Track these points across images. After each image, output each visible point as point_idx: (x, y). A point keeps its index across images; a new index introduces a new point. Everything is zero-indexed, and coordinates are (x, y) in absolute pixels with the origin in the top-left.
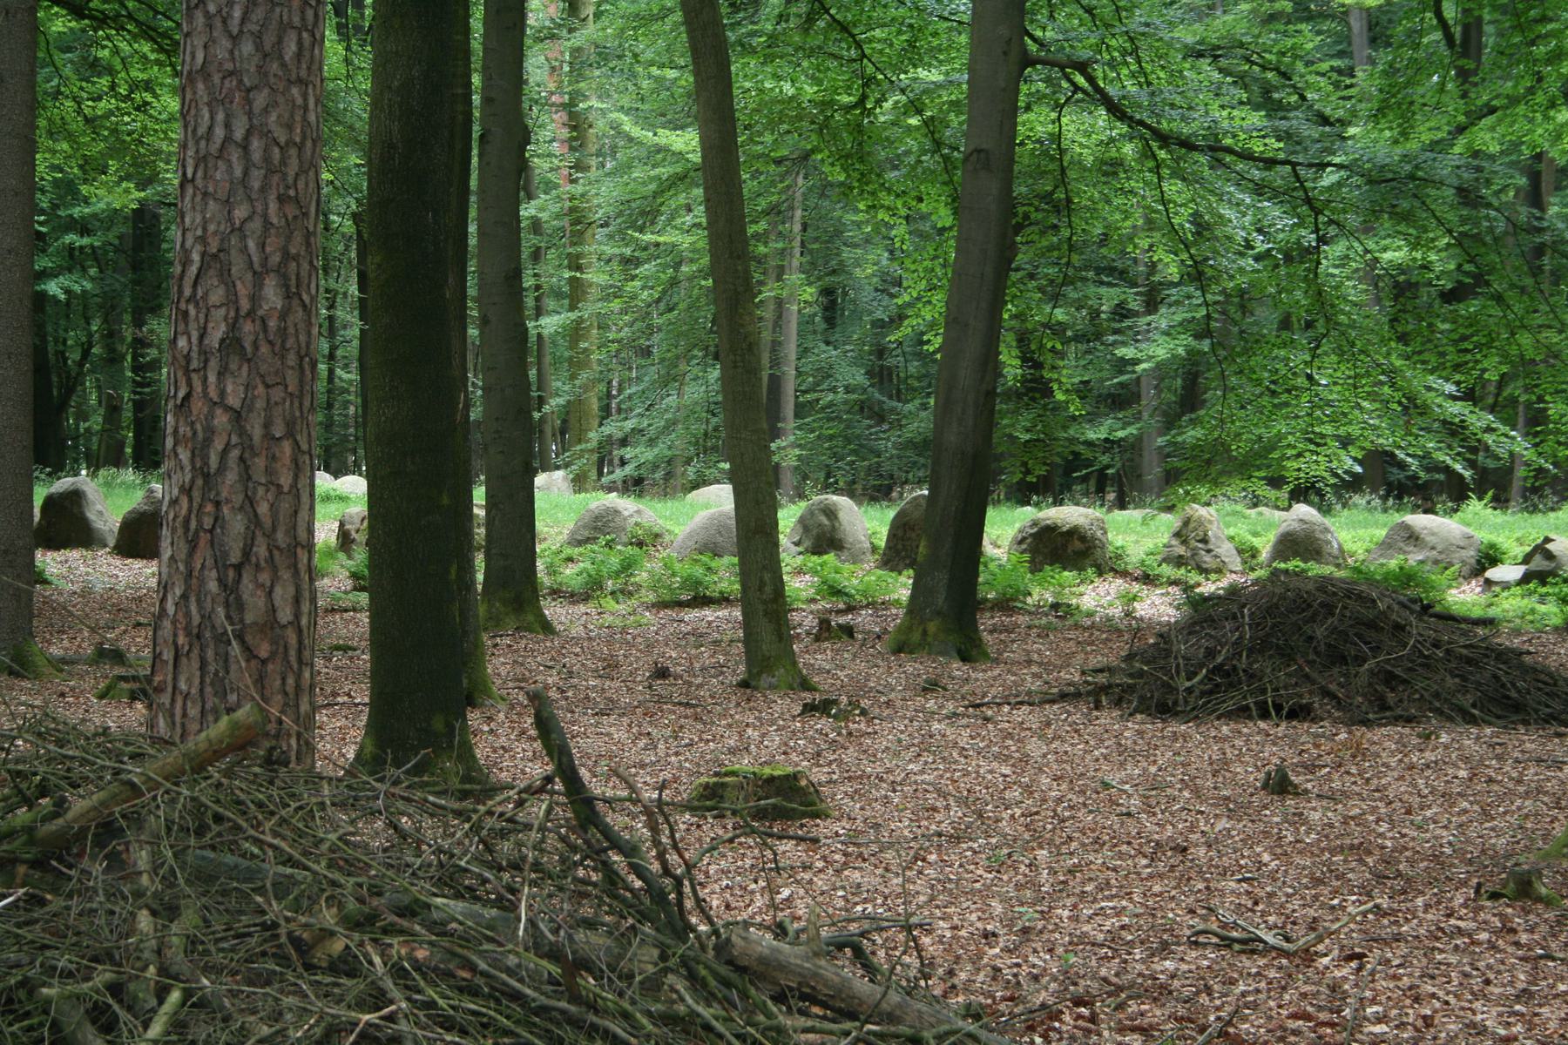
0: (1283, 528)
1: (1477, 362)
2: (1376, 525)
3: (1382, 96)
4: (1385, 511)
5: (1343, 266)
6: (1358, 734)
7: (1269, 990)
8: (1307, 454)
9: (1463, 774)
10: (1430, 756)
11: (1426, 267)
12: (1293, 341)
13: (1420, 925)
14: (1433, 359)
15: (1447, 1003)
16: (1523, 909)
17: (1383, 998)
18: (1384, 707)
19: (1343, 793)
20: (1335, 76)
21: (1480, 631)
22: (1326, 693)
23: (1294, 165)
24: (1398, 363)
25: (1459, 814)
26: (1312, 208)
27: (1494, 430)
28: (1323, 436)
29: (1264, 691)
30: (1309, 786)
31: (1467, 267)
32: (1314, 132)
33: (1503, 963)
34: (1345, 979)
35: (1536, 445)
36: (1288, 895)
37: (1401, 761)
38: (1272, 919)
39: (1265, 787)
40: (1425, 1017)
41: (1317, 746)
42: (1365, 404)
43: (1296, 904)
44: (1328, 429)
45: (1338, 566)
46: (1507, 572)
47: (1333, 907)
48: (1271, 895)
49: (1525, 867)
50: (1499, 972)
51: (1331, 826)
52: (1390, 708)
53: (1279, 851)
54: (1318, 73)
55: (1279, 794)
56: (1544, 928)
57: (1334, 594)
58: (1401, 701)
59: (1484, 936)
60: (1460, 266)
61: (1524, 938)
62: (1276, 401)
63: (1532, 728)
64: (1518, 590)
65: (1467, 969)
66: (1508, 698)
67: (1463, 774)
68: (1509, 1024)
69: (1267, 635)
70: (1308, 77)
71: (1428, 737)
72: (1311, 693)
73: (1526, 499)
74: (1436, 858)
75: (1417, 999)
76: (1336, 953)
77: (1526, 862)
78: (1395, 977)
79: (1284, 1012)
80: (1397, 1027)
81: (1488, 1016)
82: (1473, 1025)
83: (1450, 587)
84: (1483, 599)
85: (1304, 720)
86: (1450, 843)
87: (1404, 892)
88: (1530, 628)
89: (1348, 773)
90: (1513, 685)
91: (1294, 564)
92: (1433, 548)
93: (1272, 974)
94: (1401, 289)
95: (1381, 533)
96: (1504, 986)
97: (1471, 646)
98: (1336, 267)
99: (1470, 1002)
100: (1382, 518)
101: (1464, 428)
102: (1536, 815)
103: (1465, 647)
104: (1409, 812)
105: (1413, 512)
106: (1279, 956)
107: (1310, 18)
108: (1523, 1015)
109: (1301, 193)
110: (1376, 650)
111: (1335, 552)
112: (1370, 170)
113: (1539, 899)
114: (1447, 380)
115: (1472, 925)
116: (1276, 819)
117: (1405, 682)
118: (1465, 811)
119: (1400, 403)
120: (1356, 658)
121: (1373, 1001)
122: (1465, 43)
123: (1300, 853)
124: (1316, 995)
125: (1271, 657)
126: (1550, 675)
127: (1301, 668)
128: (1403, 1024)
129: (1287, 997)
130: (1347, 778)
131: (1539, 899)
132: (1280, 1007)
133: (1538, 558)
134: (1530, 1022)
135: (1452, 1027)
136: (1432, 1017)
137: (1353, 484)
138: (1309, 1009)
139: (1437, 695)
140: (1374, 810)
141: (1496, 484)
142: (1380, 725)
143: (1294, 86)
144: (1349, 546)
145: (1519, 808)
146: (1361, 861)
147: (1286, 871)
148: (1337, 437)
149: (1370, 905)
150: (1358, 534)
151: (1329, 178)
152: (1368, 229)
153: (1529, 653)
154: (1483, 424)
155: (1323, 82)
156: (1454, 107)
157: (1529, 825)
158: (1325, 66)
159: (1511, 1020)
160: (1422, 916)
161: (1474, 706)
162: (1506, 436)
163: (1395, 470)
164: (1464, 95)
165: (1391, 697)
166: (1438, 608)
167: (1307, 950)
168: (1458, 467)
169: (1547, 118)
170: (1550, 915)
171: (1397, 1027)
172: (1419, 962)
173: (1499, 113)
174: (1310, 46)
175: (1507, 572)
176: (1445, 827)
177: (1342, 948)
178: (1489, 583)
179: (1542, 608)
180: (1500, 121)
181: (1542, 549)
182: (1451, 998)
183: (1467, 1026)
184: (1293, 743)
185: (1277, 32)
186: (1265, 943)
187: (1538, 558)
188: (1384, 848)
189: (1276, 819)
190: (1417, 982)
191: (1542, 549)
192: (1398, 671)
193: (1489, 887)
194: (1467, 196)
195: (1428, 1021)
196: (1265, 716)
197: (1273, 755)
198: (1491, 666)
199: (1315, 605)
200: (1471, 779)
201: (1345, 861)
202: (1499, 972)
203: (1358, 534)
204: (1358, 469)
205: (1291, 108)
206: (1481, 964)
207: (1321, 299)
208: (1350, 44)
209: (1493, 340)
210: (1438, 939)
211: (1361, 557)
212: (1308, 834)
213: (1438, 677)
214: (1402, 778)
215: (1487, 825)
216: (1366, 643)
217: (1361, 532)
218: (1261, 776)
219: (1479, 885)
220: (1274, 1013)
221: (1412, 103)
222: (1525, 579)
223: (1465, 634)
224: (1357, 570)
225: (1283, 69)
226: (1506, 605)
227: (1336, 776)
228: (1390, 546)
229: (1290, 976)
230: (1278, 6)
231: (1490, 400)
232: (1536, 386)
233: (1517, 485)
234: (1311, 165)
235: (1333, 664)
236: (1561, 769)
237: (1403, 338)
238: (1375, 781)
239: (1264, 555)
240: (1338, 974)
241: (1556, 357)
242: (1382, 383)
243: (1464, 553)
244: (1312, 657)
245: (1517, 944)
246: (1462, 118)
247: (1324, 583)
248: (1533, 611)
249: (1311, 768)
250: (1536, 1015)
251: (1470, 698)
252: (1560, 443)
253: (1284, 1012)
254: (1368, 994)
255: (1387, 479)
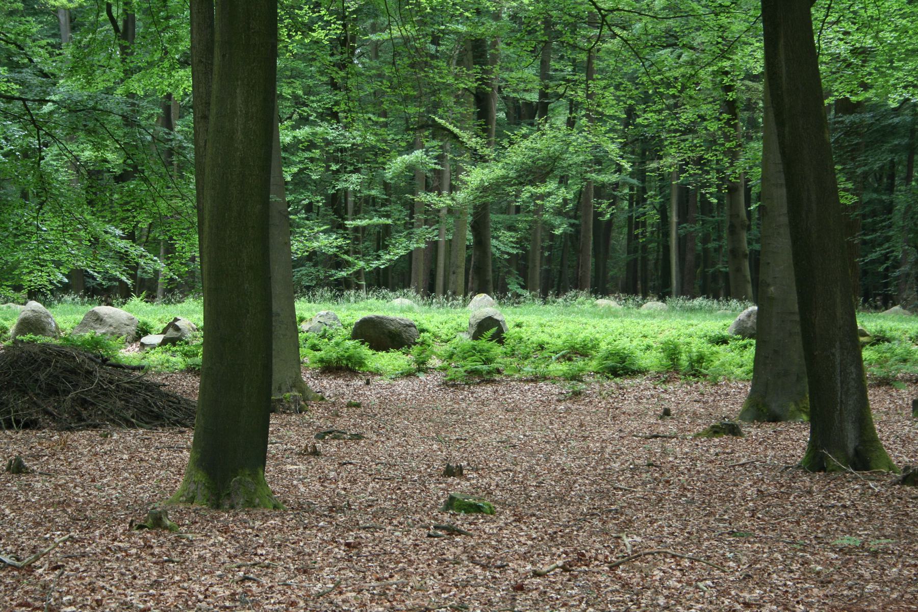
0: (22, 315)
1: (134, 217)
2: (78, 312)
3: (74, 60)
4: (83, 304)
5: (58, 160)
6: (65, 436)
7: (6, 591)
8: (35, 272)
9: (125, 457)
10: (107, 447)
11: (105, 161)
12: (26, 205)
13: (97, 546)
14: (109, 215)
15: (111, 591)
16: (156, 534)
17: (73, 591)
18: (81, 419)
19: (55, 471)
20: (49, 48)
21: (136, 373)
22: (46, 412)
23: (24, 100)
24: (88, 217)
25: (122, 480)
26: (36, 126)
27: (145, 256)
28: (45, 261)
29: (9, 413)
30: (35, 468)
31: (129, 161)
32: (36, 81)
33: (144, 566)
34: (51, 581)
35: (168, 265)
36: (19, 533)
37: (90, 451)
38: (9, 548)
39: (8, 469)
40: (97, 601)
41: (40, 444)
42: (70, 242)
43: (24, 538)
44: (47, 257)
45: (55, 337)
46: (154, 339)
47: (46, 539)
48: (9, 534)
49: (159, 509)
50: (142, 572)
51: (47, 491)
52: (84, 420)
53: (15, 507)
54: (40, 47)
55: (17, 473)
56: (168, 544)
57: (51, 354)
58: (90, 415)
59: (134, 551)
60: (125, 161)
61: (157, 551)
62: (17, 240)
63: (166, 428)
64: (159, 349)
65: (123, 570)
66: (152, 412)
67: (125, 457)
68: (146, 601)
69: (11, 379)
70: (34, 49)
71: (106, 436)
72: (37, 412)
73: (164, 296)
74: (107, 507)
75: (93, 590)
76: (47, 566)
77: (159, 506)
78: (81, 578)
79: (14, 603)
80: (81, 607)
81: (134, 598)
82: (125, 603)
83: (121, 348)
84: (141, 354)
85: (34, 428)
86: (117, 498)
87: (88, 528)
88: (166, 370)
89: (59, 459)
90: (155, 404)
91: (27, 338)
92: (111, 326)
93: (8, 581)
94: (93, 176)
95: (80, 317)
96: (144, 579)
97: (131, 382)
98: (54, 160)
99: (124, 590)
100: (81, 308)
101: (127, 255)
102: (166, 479)
103: (127, 383)
104: (93, 481)
105: (100, 305)
106: (13, 570)
107: (35, 13)
108: (154, 595)
109: (29, 118)
110: (75, 386)
111: (54, 329)
112: (69, 104)
113: (166, 528)
114: (117, 228)
115: (128, 545)
116: (15, 488)
117: (92, 404)
118: (126, 479)
119: (90, 241)
120: (64, 391)
121: (68, 593)
122: (126, 33)
123: (28, 507)
124: (33, 592)
125: (13, 392)
126: (176, 397)
127: (31, 398)
128: (84, 605)
129: (16, 594)
130: (58, 462)
131: (166, 528)
132: (12, 600)
133: (171, 330)
134: (158, 599)
135: (113, 605)
136: (101, 600)
137: (65, 289)
138: (29, 600)
139: (111, 412)
140: (73, 480)
141: (147, 288)
142: (78, 431)
143: (25, 54)
144: (61, 325)
145: (157, 476)
146: (64, 511)
147: (19, 519)
148: (53, 262)
149: (67, 536)
150: (67, 318)
151: (48, 108)
152: (72, 139)
153: (164, 385)
154: (139, 253)
155: (42, 51)
156: (117, 71)
157: (163, 485)
158: (44, 42)
159: (147, 599)
160: (99, 540)
161: (133, 417)
162: (152, 260)
163: (91, 280)
164: (123, 60)
165: (85, 414)
166: (113, 361)
167: (30, 565)
168: (124, 278)
169: (170, 75)
170: (172, 537)
171: (81, 607)
172: (96, 568)
173: (143, 72)
174: (34, 30)
175: (154, 339)
176: (114, 488)
177: (50, 563)
178: (143, 345)
179: (173, 359)
180: (143, 77)
181: (173, 325)
182: (113, 588)
183: (122, 604)
184: (27, 442)
185: (15, 21)
186: (4, 562)
187: (171, 330)
188: (77, 502)
189: (15, 488)
190: (94, 580)
191: (173, 325)
192: (89, 398)
193: (138, 522)
194: (129, 121)
195: (99, 603)
196: (10, 427)
197: (14, 450)
198: (143, 394)
199: (39, 360)
200: (130, 460)
201: (55, 511)
202: (142, 572)
203: (67, 318)
204: (66, 280)
205: (25, 66)
206: (132, 568)
207: (43, 181)
208: (59, 30)
209: (143, 204)
210: (107, 554)
211: (69, 332)
212: (33, 496)
213: (112, 401)
214: (90, 461)
215: (139, 486)
216: (69, 382)
217: (69, 317)
218: (6, 463)
219: (132, 521)
220: (8, 604)
221: (93, 65)
222: (164, 343)
223: (128, 375)
224: (66, 339)
225: (19, 43)
226: (152, 358)
227: (51, 461)
228: (86, 325)
229: (19, 581)
230: (15, 6)
231: (144, 239)
232: (168, 231)
233: (160, 287)
234: (34, 101)
235: (50, 395)
236: (182, 452)
237: (91, 203)
238: (75, 463)
239: (11, 332)
240: (47, 578)
241: (180, 214)
242: (79, 230)
243: (128, 328)
244: (38, 391)
245: (152, 554)
246: (121, 75)
247: (45, 347)
248: (168, 361)
249: (37, 457)
250: (161, 595)
251: (130, 413)
252: (181, 264)
253: (14, 603)
254: (65, 589)
255: (84, 286)
